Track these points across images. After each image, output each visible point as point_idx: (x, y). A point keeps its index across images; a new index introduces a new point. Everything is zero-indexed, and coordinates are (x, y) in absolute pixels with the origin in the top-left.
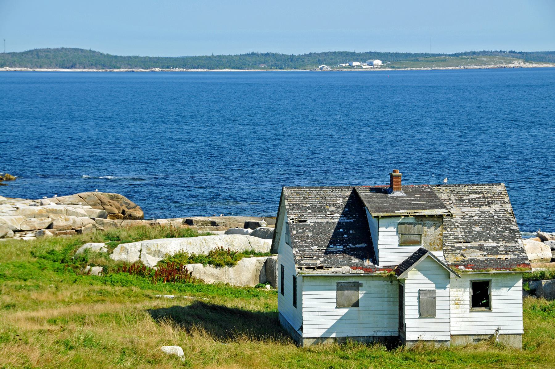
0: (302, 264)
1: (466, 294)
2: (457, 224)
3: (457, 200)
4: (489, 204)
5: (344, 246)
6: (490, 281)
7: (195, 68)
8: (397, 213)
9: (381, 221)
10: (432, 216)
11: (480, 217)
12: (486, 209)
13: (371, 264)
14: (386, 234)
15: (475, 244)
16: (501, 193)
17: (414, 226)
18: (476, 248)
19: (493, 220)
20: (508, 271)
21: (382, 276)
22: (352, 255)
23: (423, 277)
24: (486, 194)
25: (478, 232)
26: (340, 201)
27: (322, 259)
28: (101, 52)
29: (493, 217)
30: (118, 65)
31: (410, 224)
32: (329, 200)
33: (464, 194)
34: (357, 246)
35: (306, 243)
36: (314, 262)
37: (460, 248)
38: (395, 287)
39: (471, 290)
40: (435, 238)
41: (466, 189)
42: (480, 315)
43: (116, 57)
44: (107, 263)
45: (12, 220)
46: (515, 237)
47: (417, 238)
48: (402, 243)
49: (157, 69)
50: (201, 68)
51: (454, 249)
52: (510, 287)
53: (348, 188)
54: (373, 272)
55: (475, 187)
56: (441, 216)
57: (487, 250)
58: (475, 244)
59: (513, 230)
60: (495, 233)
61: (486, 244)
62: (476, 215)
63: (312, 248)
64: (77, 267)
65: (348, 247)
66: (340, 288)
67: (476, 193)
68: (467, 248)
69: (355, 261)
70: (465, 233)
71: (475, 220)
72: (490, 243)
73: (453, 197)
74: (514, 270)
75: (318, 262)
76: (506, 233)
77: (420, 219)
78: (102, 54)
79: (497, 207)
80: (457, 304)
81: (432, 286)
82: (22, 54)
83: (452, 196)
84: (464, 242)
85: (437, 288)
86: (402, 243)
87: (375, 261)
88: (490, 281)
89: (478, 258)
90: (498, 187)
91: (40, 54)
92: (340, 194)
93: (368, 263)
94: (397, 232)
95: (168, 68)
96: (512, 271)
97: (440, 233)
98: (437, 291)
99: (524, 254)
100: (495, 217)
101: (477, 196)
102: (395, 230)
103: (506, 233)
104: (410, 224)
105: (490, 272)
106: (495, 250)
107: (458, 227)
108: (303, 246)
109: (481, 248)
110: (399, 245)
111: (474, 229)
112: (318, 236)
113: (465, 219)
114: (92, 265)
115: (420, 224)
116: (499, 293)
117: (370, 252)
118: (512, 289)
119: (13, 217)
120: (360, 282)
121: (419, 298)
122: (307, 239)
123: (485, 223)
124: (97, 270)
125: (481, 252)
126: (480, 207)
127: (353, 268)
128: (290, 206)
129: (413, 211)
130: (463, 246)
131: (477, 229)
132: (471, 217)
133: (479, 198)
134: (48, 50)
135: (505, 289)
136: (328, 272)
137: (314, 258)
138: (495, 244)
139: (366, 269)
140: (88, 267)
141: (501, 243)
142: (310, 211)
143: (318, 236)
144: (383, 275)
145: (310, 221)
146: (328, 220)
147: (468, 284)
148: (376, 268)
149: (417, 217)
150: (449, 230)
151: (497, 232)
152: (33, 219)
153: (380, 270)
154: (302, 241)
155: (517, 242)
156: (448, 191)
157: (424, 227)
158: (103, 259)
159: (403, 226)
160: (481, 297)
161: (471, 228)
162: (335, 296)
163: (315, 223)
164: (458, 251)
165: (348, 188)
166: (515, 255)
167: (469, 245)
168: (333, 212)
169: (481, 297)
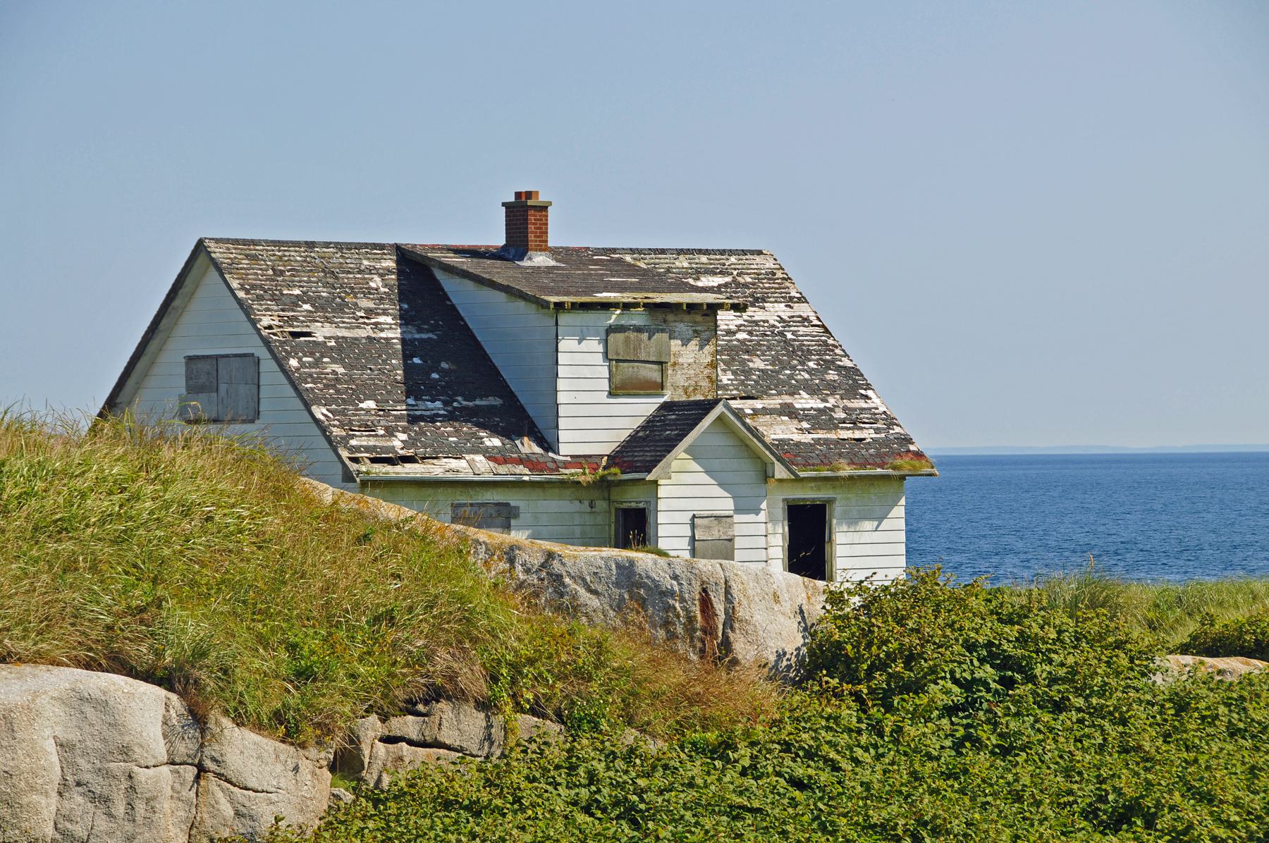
5: (445, 403)
6: (831, 501)
9: (564, 319)
11: (750, 333)
13: (538, 450)
14: (578, 359)
16: (774, 274)
17: (650, 338)
19: (787, 342)
21: (579, 483)
22: (482, 426)
23: (706, 478)
24: (739, 275)
27: (404, 437)
29: (781, 334)
31: (639, 330)
34: (478, 402)
35: (338, 391)
38: (599, 520)
40: (696, 375)
47: (652, 373)
48: (618, 389)
52: (881, 519)
57: (806, 418)
58: (774, 402)
59: (845, 368)
63: (361, 405)
65: (455, 404)
67: (715, 274)
70: (734, 373)
74: (894, 468)
81: (725, 504)
84: (742, 398)
85: (738, 510)
86: (618, 389)
87: (549, 445)
88: (831, 501)
92: (366, 262)
94: (606, 354)
96: (890, 472)
97: (709, 359)
98: (737, 518)
102: (601, 348)
103: (832, 375)
104: (639, 330)
105: (842, 473)
106: (821, 419)
109: (789, 412)
110: (611, 394)
111: (751, 365)
115: (663, 331)
116: (856, 537)
117: (519, 415)
118: (886, 524)
120: (513, 503)
121: (693, 539)
123: (769, 349)
128: (247, 292)
133: (726, 285)
135: (868, 525)
137: (381, 432)
144: (581, 479)
147: (780, 511)
148: (554, 461)
149: (652, 307)
153: (566, 465)
154: (327, 386)
155: (867, 397)
157: (673, 342)
159: (620, 336)
161: (743, 362)
163: (337, 338)
166: (877, 431)
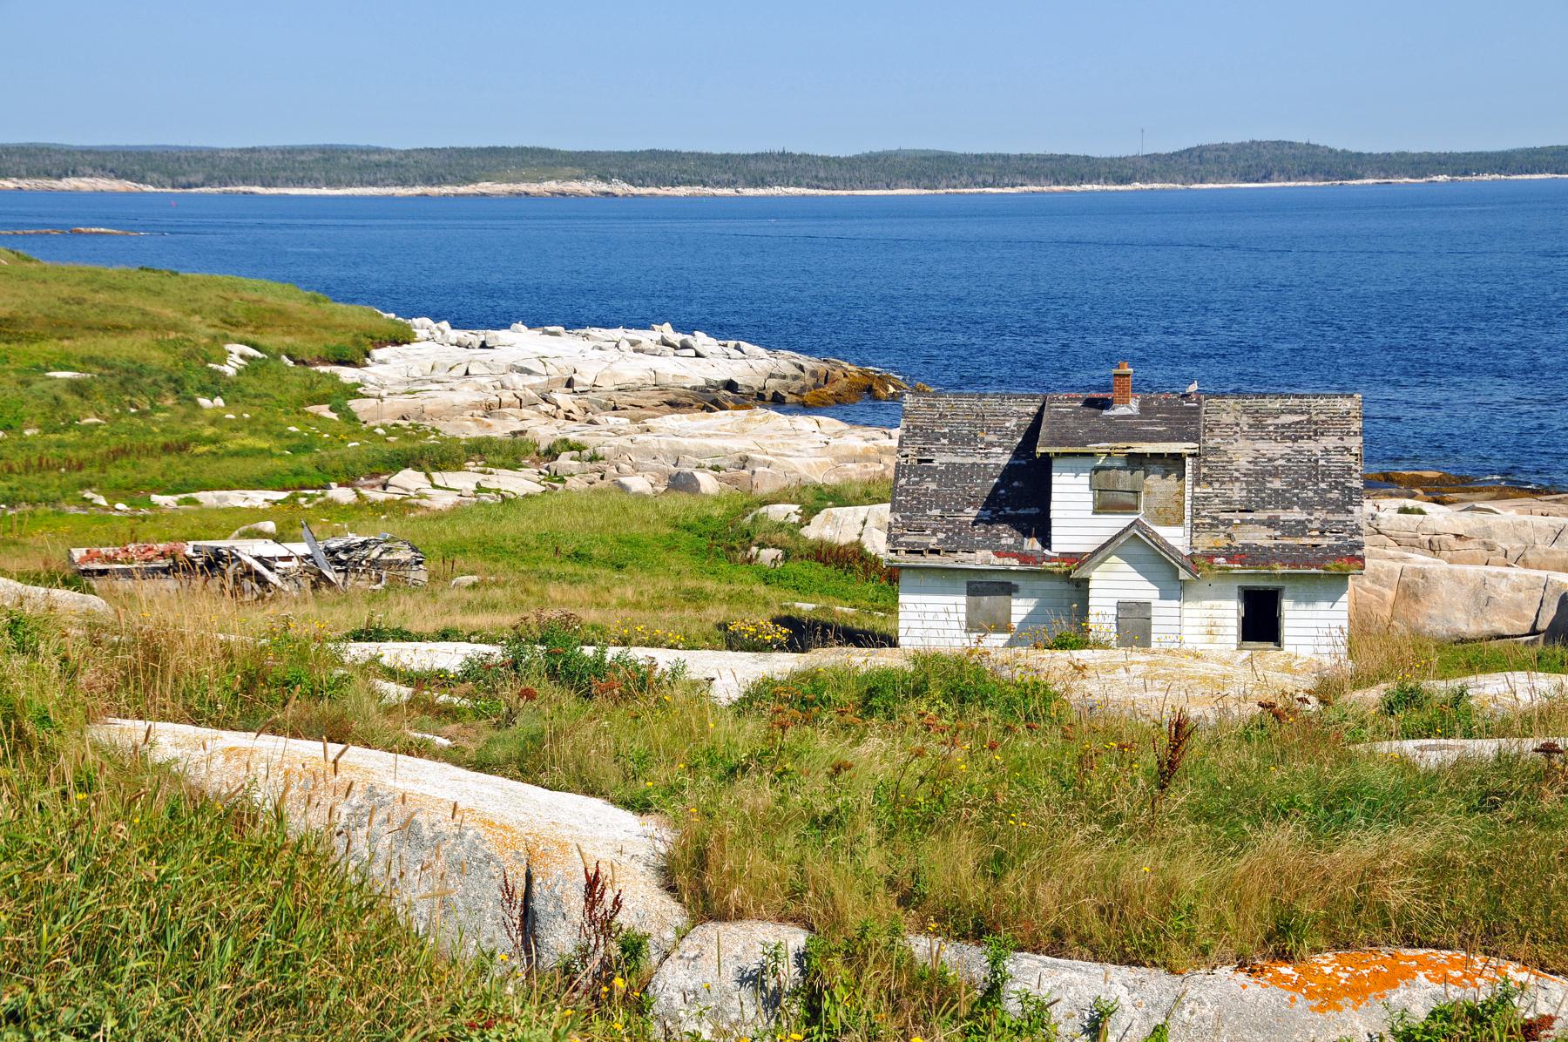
0: (901, 544)
1: (1230, 611)
2: (1236, 474)
3: (1250, 426)
4: (1317, 434)
6: (1282, 589)
7: (1527, 172)
8: (1091, 448)
10: (1161, 455)
12: (1305, 445)
13: (1038, 546)
15: (1262, 515)
18: (1262, 523)
20: (1314, 570)
25: (1276, 491)
26: (1011, 424)
28: (1331, 146)
30: (1359, 172)
32: (990, 420)
33: (1270, 414)
36: (925, 540)
37: (1229, 523)
39: (1241, 607)
41: (1277, 404)
42: (1267, 654)
43: (1359, 155)
44: (791, 544)
45: (809, 465)
46: (1350, 502)
47: (1130, 499)
48: (1102, 508)
49: (1441, 178)
50: (1541, 172)
51: (1215, 524)
53: (1034, 397)
54: (1036, 563)
55: (1297, 401)
56: (1178, 458)
58: (1262, 515)
60: (1311, 494)
61: (1285, 516)
62: (1282, 457)
64: (734, 548)
66: (974, 590)
68: (1243, 522)
69: (1007, 540)
70: (1250, 491)
71: (1276, 468)
72: (1296, 514)
73: (1245, 420)
75: (934, 540)
76: (1335, 494)
77: (1137, 461)
78: (1331, 151)
79: (1329, 442)
80: (1210, 633)
82: (1171, 156)
83: (1245, 418)
86: (1102, 508)
87: (1046, 542)
89: (1259, 543)
90: (1345, 401)
91: (1207, 155)
93: (1032, 544)
95: (1466, 173)
99: (1357, 538)
100: (1321, 462)
101: (1297, 418)
103: (1335, 494)
104: (1119, 469)
106: (1301, 528)
107: (1237, 479)
108: (911, 510)
109: (1271, 523)
110: (1094, 513)
112: (946, 491)
113: (1256, 464)
114: (761, 546)
119: (811, 461)
122: (925, 495)
124: (768, 554)
125: (1271, 532)
126: (1295, 441)
127: (999, 555)
129: (1125, 445)
130: (1236, 518)
131: (1277, 484)
132: (1270, 460)
134: (1223, 148)
136: (948, 561)
138: (1303, 516)
139: (1024, 558)
140: (754, 549)
141: (1317, 514)
142: (945, 441)
143: (946, 491)
145: (940, 460)
146: (977, 460)
150: (1217, 485)
151: (1315, 492)
152: (850, 466)
153: (1051, 559)
156: (1238, 407)
158: (785, 535)
160: (1261, 622)
162: (963, 609)
164: (1222, 528)
165: (1034, 397)
167: (1249, 516)
168: (991, 444)
169: (1261, 622)
